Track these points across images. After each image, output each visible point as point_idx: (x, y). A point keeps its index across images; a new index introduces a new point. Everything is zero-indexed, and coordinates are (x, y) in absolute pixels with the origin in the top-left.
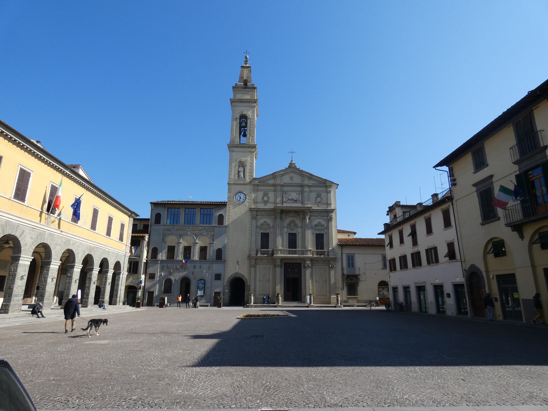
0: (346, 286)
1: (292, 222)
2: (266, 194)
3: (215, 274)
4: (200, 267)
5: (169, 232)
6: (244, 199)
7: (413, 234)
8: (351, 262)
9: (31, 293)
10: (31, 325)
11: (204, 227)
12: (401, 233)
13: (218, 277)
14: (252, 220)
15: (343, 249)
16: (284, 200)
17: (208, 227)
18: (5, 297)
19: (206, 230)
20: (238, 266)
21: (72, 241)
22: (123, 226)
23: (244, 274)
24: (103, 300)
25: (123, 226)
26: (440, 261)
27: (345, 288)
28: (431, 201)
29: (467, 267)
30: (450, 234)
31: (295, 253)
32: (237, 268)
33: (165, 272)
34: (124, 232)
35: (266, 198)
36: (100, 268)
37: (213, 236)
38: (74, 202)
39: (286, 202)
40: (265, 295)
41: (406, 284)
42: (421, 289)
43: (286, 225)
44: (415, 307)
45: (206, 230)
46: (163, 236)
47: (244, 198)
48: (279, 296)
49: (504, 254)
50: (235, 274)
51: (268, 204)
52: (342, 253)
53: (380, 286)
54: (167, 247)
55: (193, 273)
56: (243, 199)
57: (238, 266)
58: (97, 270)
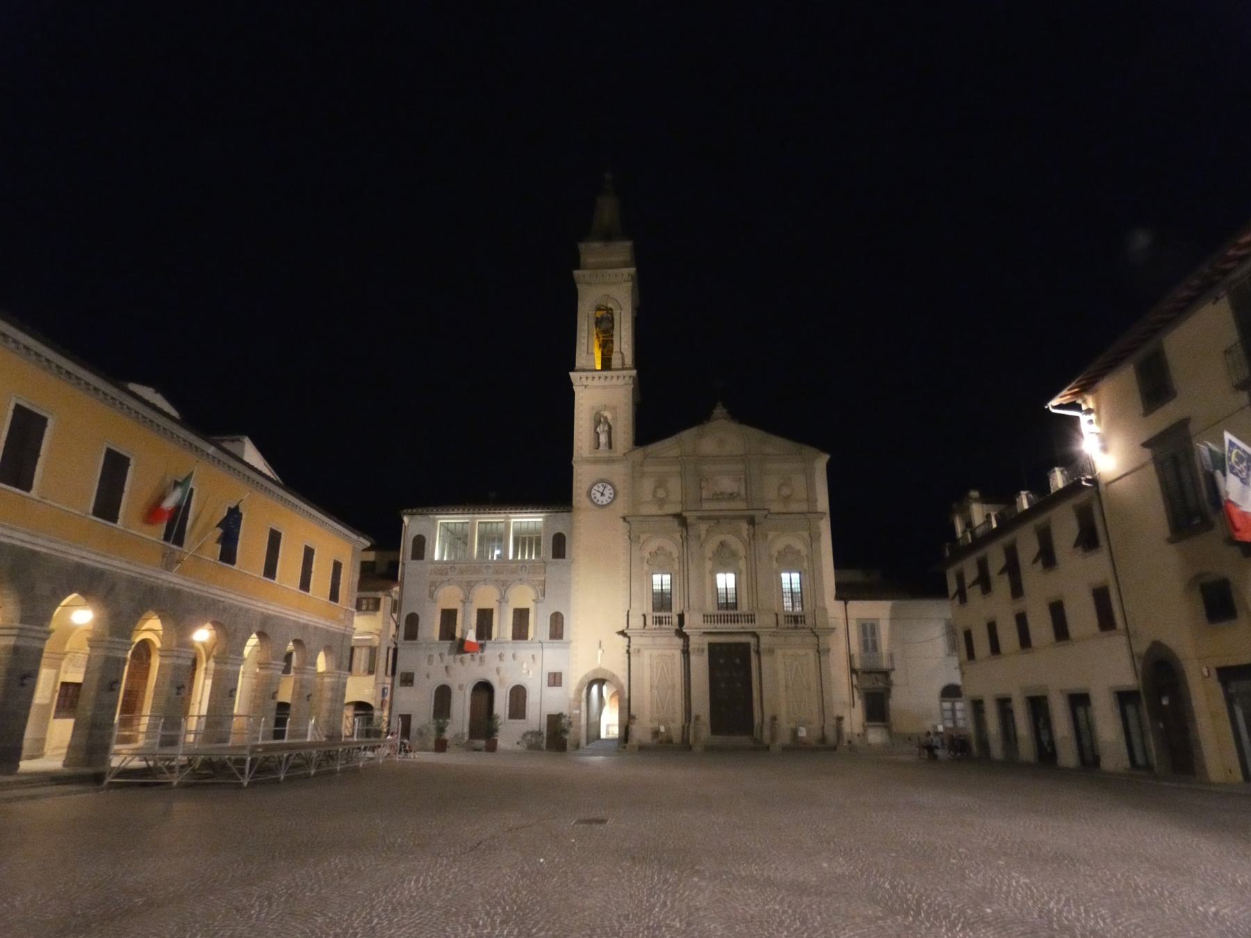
0: (859, 698)
1: (722, 544)
2: (661, 484)
5: (444, 578)
6: (612, 496)
7: (1012, 568)
8: (870, 639)
9: (139, 722)
11: (521, 565)
12: (983, 565)
13: (555, 679)
17: (531, 564)
18: (400, 586)
19: (526, 570)
20: (600, 652)
21: (222, 604)
23: (615, 672)
25: (337, 567)
26: (1034, 643)
27: (859, 703)
29: (1142, 647)
30: (1095, 568)
31: (751, 620)
34: (341, 581)
35: (661, 493)
36: (285, 664)
37: (544, 583)
38: (225, 514)
39: (707, 500)
41: (1001, 691)
42: (1038, 705)
44: (997, 750)
45: (526, 570)
46: (430, 586)
47: (611, 494)
48: (196, 733)
49: (560, 685)
50: (595, 671)
51: (666, 507)
52: (847, 619)
53: (279, 726)
56: (609, 498)
57: (600, 652)
58: (279, 667)
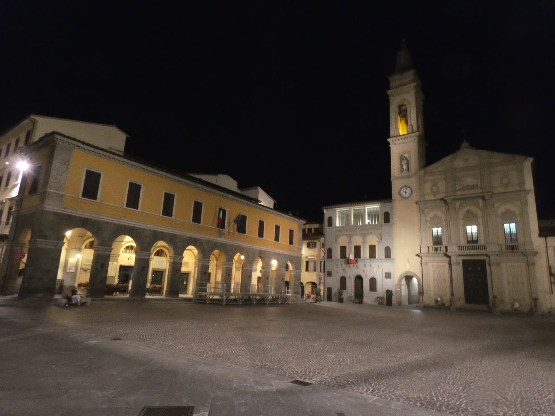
3: (385, 273)
4: (370, 266)
6: (402, 196)
10: (292, 364)
14: (420, 214)
15: (547, 240)
16: (458, 187)
22: (291, 232)
24: (175, 256)
25: (291, 232)
28: (188, 248)
32: (408, 266)
33: (136, 248)
40: (438, 296)
43: (429, 219)
46: (335, 237)
50: (406, 272)
54: (354, 246)
55: (364, 271)
57: (408, 264)
